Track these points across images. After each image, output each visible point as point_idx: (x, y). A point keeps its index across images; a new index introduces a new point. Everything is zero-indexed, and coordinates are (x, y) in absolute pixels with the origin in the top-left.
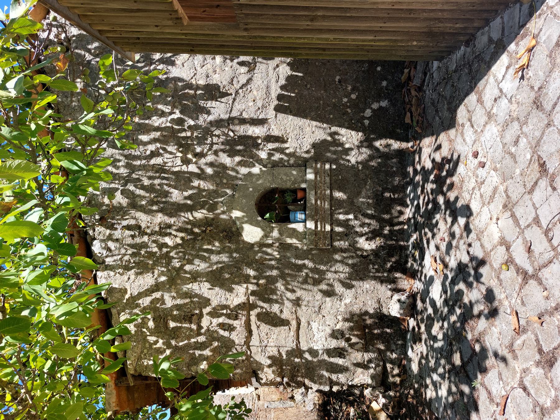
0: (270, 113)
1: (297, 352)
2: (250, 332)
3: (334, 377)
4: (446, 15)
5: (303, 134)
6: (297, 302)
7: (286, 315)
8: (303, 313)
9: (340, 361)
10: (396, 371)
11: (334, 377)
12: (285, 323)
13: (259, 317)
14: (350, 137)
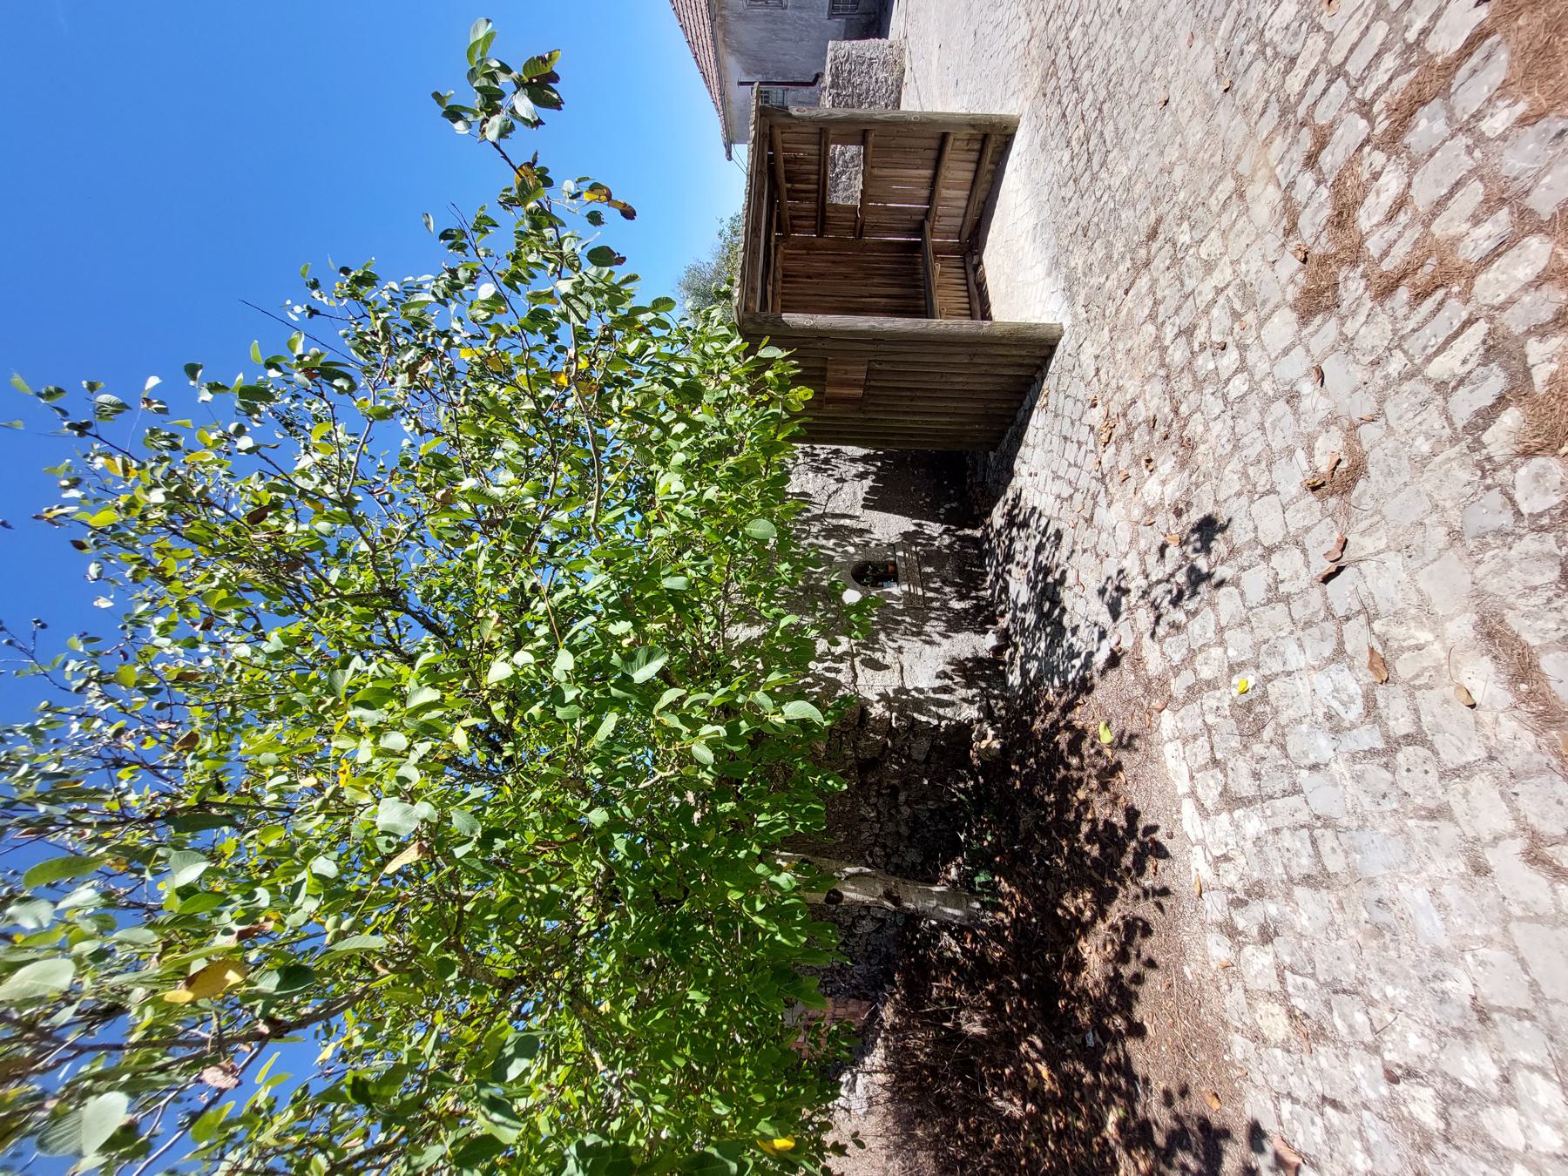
0: (858, 512)
1: (902, 690)
2: (856, 676)
3: (941, 711)
4: (995, 396)
5: (889, 527)
6: (900, 650)
7: (888, 660)
8: (906, 659)
9: (945, 697)
10: (1001, 704)
11: (941, 711)
12: (887, 667)
13: (862, 662)
14: (933, 529)
